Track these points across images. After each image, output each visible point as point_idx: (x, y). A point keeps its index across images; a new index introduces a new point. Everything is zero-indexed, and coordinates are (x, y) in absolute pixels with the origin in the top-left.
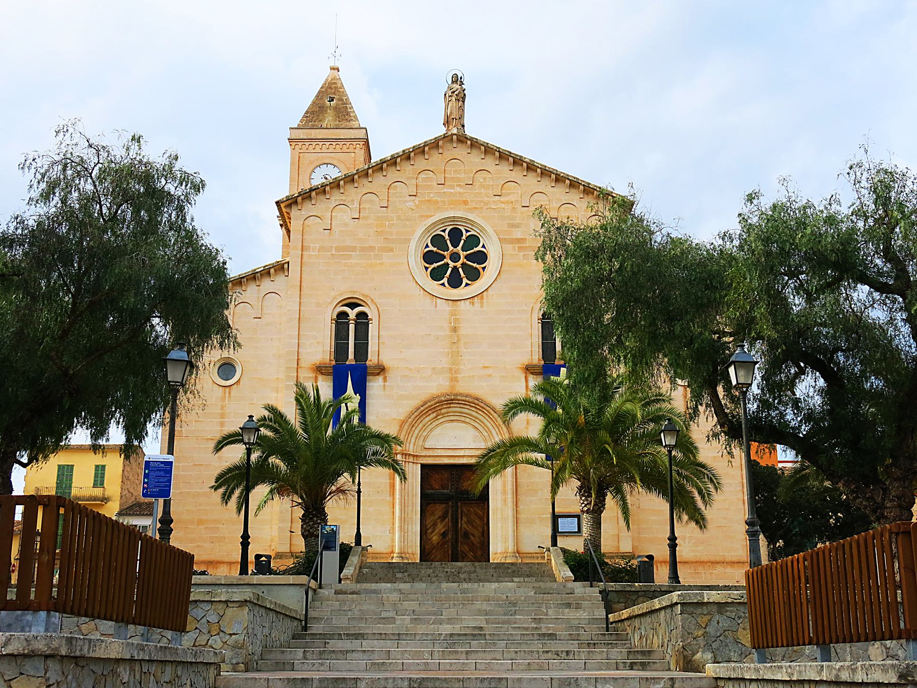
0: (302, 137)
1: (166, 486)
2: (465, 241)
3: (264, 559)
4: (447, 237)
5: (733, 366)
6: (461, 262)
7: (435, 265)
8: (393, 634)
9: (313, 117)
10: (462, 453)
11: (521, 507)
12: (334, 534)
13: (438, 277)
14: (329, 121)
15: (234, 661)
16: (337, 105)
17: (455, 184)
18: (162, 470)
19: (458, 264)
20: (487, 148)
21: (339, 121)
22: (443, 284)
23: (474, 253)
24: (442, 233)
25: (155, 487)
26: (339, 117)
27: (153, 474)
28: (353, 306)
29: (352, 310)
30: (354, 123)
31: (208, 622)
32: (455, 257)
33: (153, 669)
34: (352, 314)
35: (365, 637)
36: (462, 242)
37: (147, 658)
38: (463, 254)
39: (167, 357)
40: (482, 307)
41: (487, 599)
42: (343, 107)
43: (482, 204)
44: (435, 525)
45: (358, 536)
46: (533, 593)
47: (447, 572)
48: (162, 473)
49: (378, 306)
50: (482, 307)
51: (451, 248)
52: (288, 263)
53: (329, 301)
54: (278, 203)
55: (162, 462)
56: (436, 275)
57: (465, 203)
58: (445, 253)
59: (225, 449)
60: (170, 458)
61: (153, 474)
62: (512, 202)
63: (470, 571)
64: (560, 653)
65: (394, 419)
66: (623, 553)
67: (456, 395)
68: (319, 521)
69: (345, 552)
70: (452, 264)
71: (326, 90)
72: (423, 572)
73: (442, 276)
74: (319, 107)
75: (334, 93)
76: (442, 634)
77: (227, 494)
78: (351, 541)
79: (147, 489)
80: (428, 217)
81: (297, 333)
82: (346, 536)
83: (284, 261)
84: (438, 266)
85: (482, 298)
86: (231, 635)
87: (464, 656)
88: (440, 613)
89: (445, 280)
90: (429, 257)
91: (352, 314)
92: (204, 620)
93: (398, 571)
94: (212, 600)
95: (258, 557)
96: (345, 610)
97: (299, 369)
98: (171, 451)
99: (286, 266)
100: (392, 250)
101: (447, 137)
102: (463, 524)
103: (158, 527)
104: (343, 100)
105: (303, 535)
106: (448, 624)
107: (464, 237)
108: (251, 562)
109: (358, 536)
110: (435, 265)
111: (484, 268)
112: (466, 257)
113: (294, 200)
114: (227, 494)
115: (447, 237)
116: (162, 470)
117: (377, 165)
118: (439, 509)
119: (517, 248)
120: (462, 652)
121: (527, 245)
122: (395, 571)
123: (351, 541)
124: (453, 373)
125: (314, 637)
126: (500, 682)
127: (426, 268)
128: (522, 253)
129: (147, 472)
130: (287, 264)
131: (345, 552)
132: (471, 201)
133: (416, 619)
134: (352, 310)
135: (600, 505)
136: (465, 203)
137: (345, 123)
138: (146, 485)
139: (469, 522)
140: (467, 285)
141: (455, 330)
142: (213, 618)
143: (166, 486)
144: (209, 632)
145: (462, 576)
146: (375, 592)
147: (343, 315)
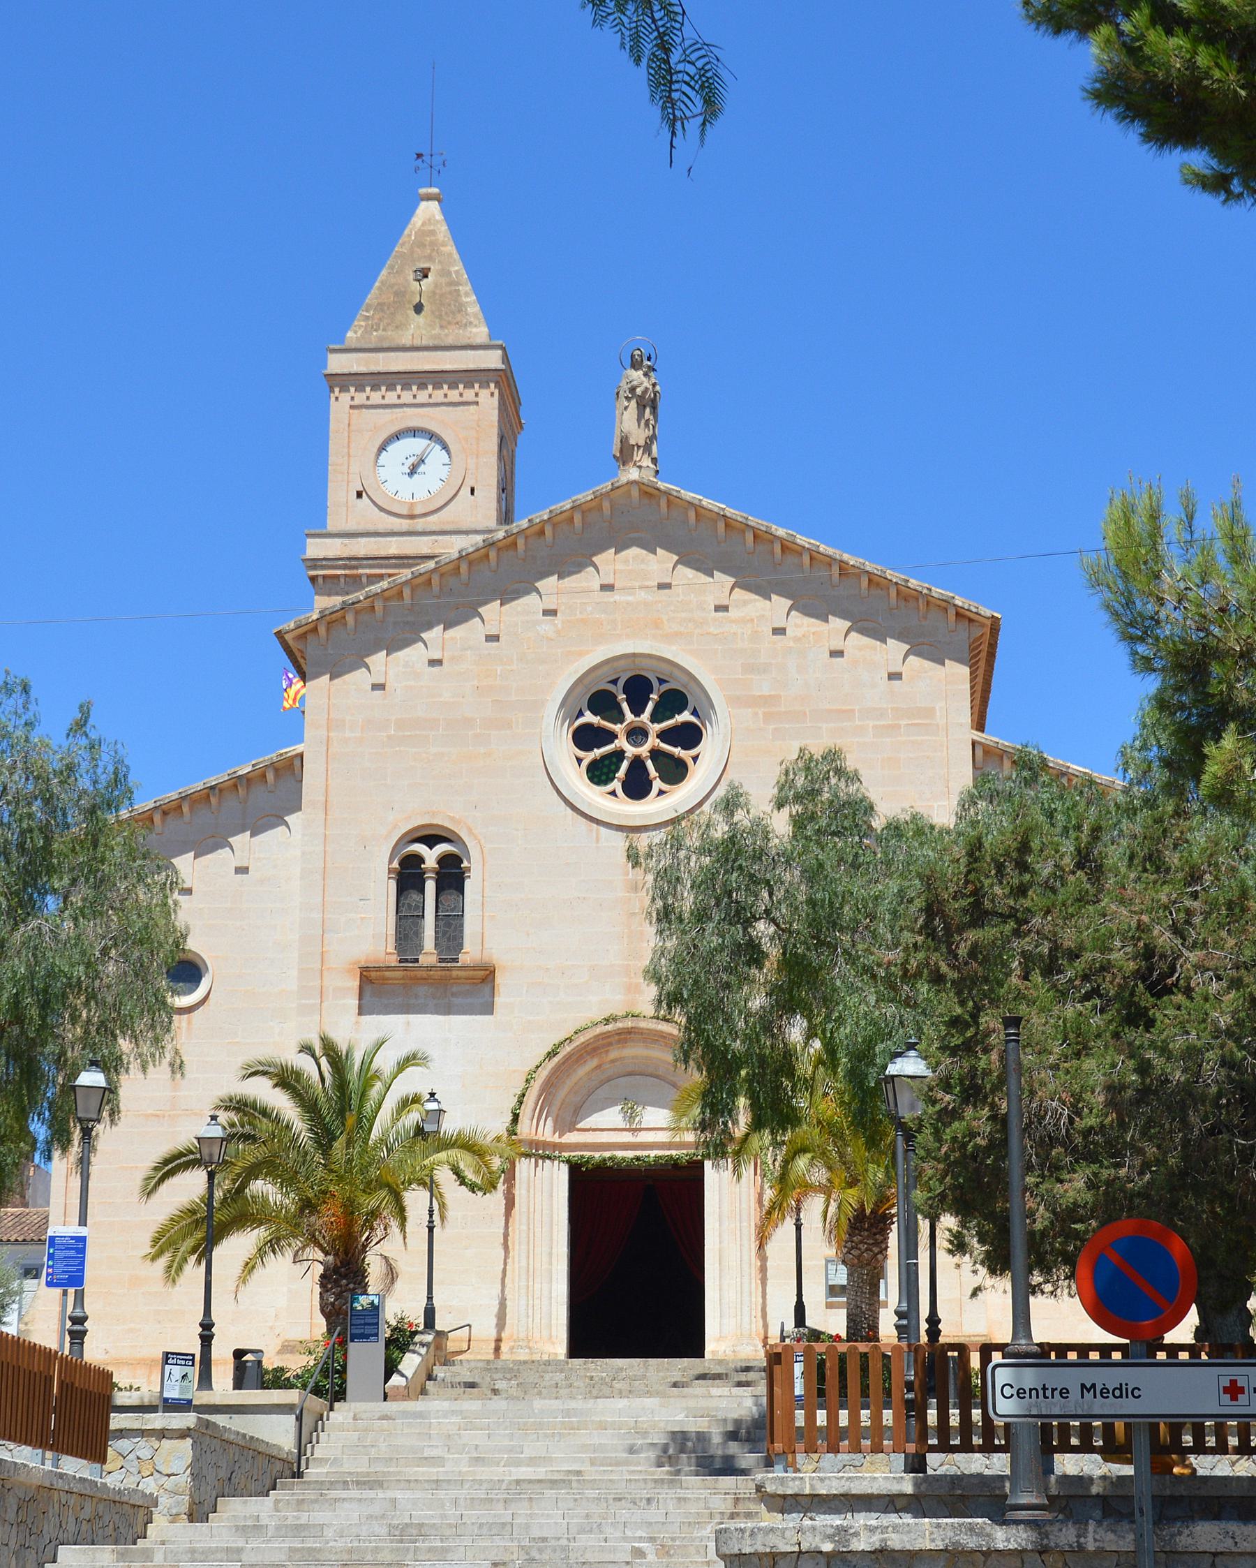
1: (78, 1271)
3: (249, 1357)
7: (621, 773)
8: (428, 1481)
9: (380, 319)
13: (604, 778)
14: (418, 327)
15: (174, 1511)
16: (436, 286)
18: (72, 1249)
20: (698, 508)
21: (442, 327)
25: (63, 1272)
26: (440, 317)
29: (431, 849)
30: (474, 330)
31: (138, 1458)
33: (72, 1501)
34: (431, 856)
35: (385, 1486)
37: (66, 1488)
38: (644, 751)
39: (77, 1083)
41: (603, 1426)
42: (450, 293)
43: (690, 625)
45: (430, 1313)
46: (683, 1415)
47: (592, 1378)
48: (72, 1253)
49: (483, 842)
51: (629, 716)
54: (54, 1561)
55: (72, 1238)
56: (599, 773)
59: (164, 1187)
60: (82, 1231)
62: (752, 620)
63: (635, 1376)
64: (638, 1501)
65: (514, 1071)
66: (970, 1336)
68: (351, 1286)
69: (400, 1341)
71: (412, 252)
72: (547, 1377)
73: (611, 775)
74: (396, 294)
75: (430, 258)
76: (503, 1481)
77: (175, 1265)
79: (52, 1275)
80: (581, 654)
81: (320, 899)
83: (294, 753)
84: (604, 757)
86: (169, 1476)
87: (501, 1504)
88: (518, 1450)
91: (431, 856)
92: (131, 1456)
93: (501, 1376)
94: (143, 1428)
95: (239, 1354)
96: (365, 1447)
97: (325, 973)
98: (83, 1221)
99: (297, 762)
101: (618, 488)
103: (67, 1327)
104: (450, 273)
105: (322, 1311)
106: (528, 1465)
108: (225, 1363)
109: (430, 1313)
110: (621, 773)
111: (695, 759)
113: (312, 625)
114: (175, 1265)
116: (72, 1249)
117: (477, 550)
119: (761, 716)
120: (498, 1500)
121: (783, 709)
122: (495, 1376)
124: (633, 975)
125: (307, 1486)
126: (503, 1528)
127: (579, 761)
128: (771, 727)
129: (51, 1251)
130: (299, 758)
131: (400, 1341)
133: (477, 1459)
134: (431, 849)
135: (876, 1250)
138: (50, 1270)
140: (661, 792)
142: (145, 1453)
143: (78, 1271)
144: (139, 1472)
145: (617, 1385)
146: (420, 1415)
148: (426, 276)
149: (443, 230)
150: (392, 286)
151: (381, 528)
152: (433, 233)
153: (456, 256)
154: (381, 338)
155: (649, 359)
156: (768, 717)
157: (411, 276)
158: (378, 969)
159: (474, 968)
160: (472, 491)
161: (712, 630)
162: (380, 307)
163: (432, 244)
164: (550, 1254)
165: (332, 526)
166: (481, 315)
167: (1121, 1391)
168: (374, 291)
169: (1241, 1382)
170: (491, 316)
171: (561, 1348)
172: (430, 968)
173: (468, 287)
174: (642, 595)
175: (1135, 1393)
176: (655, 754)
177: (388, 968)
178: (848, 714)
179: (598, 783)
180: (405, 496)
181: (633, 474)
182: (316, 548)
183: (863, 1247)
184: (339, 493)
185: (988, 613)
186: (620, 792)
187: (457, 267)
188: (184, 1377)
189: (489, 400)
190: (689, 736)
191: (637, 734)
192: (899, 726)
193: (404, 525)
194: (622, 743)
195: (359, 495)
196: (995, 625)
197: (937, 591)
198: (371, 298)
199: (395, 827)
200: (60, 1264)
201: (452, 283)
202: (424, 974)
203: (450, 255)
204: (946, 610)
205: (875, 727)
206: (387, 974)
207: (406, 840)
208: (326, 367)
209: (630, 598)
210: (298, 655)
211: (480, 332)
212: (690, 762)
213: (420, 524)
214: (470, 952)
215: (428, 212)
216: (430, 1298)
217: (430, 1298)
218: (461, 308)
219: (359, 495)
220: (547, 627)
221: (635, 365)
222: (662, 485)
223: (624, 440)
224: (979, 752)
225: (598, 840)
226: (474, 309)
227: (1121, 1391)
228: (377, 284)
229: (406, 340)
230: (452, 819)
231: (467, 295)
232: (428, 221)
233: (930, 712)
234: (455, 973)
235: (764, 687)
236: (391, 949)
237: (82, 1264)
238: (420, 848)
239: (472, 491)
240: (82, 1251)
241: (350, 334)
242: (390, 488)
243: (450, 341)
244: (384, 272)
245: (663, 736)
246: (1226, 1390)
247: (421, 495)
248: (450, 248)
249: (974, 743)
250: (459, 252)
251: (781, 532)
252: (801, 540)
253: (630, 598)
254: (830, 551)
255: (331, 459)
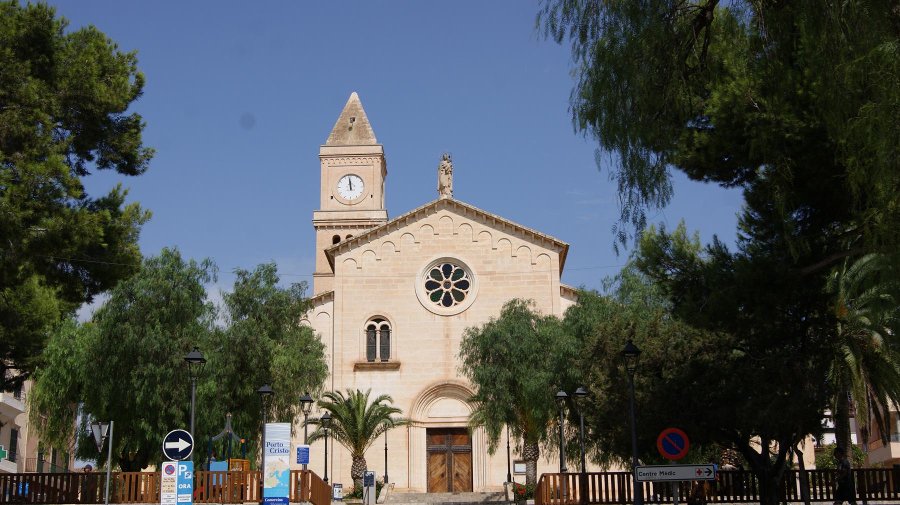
0: (330, 154)
2: (454, 274)
4: (441, 271)
5: (566, 395)
6: (451, 289)
7: (434, 291)
10: (454, 420)
11: (412, 475)
12: (372, 476)
17: (446, 234)
19: (449, 290)
22: (439, 304)
23: (459, 291)
24: (438, 268)
26: (359, 135)
27: (301, 453)
28: (378, 320)
32: (447, 285)
34: (378, 326)
36: (452, 274)
38: (453, 287)
40: (466, 319)
44: (436, 469)
50: (466, 319)
51: (444, 279)
52: (334, 292)
53: (362, 318)
56: (435, 298)
57: (454, 247)
58: (440, 282)
61: (301, 453)
67: (449, 381)
70: (445, 290)
72: (427, 498)
75: (355, 114)
78: (382, 480)
80: (429, 257)
82: (379, 476)
84: (436, 292)
85: (466, 314)
89: (441, 301)
90: (430, 286)
91: (378, 326)
99: (332, 294)
100: (403, 281)
102: (456, 469)
104: (362, 120)
107: (453, 271)
109: (386, 478)
110: (434, 291)
111: (467, 292)
112: (453, 290)
115: (441, 271)
118: (439, 458)
123: (382, 480)
127: (428, 293)
132: (458, 246)
136: (454, 247)
137: (363, 142)
139: (459, 466)
140: (456, 304)
141: (447, 336)
147: (372, 328)
148: (354, 121)
149: (359, 104)
150: (342, 124)
151: (340, 209)
152: (356, 105)
153: (364, 114)
154: (338, 143)
155: (449, 157)
156: (491, 279)
157: (349, 121)
158: (361, 364)
159: (394, 364)
160: (372, 196)
161: (472, 249)
162: (338, 131)
163: (356, 109)
164: (421, 460)
165: (322, 209)
166: (374, 134)
167: (670, 473)
168: (336, 126)
169: (701, 470)
170: (377, 135)
171: (425, 491)
172: (379, 364)
173: (369, 125)
174: (448, 238)
175: (674, 474)
176: (441, 291)
177: (364, 364)
178: (519, 278)
179: (434, 301)
180: (348, 198)
181: (445, 197)
182: (317, 216)
183: (531, 455)
184: (325, 197)
185: (565, 244)
186: (442, 304)
187: (365, 118)
188: (340, 491)
189: (377, 163)
190: (465, 285)
191: (447, 285)
192: (535, 282)
193: (347, 208)
194: (442, 287)
195: (332, 197)
196: (567, 247)
197: (548, 237)
198: (335, 128)
199: (366, 316)
200: (301, 456)
201: (363, 123)
202: (377, 365)
203: (362, 113)
204: (551, 242)
205: (528, 282)
206: (364, 366)
207: (374, 319)
208: (319, 153)
209: (444, 239)
210: (331, 257)
211: (374, 141)
212: (465, 294)
213: (353, 208)
214: (393, 358)
215: (354, 96)
216: (386, 473)
217: (386, 473)
218: (367, 132)
219: (332, 197)
220: (416, 248)
221: (444, 159)
222: (455, 200)
223: (441, 185)
224: (563, 290)
225: (435, 320)
226: (371, 132)
227: (670, 473)
228: (337, 123)
229: (347, 144)
230: (385, 313)
231: (368, 127)
232: (354, 101)
233: (546, 277)
234: (387, 365)
235: (489, 268)
236: (365, 356)
237: (308, 456)
238: (374, 323)
239: (372, 196)
240: (308, 452)
241: (328, 141)
242: (343, 195)
243: (363, 144)
244: (339, 120)
245: (456, 285)
246: (697, 472)
247: (354, 198)
248: (362, 111)
249: (561, 287)
250: (365, 112)
251: (495, 216)
252: (502, 219)
253: (444, 239)
254: (512, 223)
255: (322, 185)
